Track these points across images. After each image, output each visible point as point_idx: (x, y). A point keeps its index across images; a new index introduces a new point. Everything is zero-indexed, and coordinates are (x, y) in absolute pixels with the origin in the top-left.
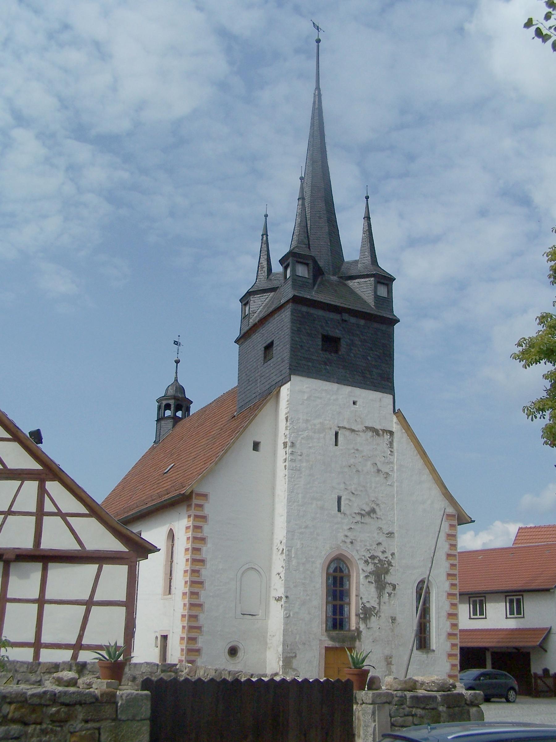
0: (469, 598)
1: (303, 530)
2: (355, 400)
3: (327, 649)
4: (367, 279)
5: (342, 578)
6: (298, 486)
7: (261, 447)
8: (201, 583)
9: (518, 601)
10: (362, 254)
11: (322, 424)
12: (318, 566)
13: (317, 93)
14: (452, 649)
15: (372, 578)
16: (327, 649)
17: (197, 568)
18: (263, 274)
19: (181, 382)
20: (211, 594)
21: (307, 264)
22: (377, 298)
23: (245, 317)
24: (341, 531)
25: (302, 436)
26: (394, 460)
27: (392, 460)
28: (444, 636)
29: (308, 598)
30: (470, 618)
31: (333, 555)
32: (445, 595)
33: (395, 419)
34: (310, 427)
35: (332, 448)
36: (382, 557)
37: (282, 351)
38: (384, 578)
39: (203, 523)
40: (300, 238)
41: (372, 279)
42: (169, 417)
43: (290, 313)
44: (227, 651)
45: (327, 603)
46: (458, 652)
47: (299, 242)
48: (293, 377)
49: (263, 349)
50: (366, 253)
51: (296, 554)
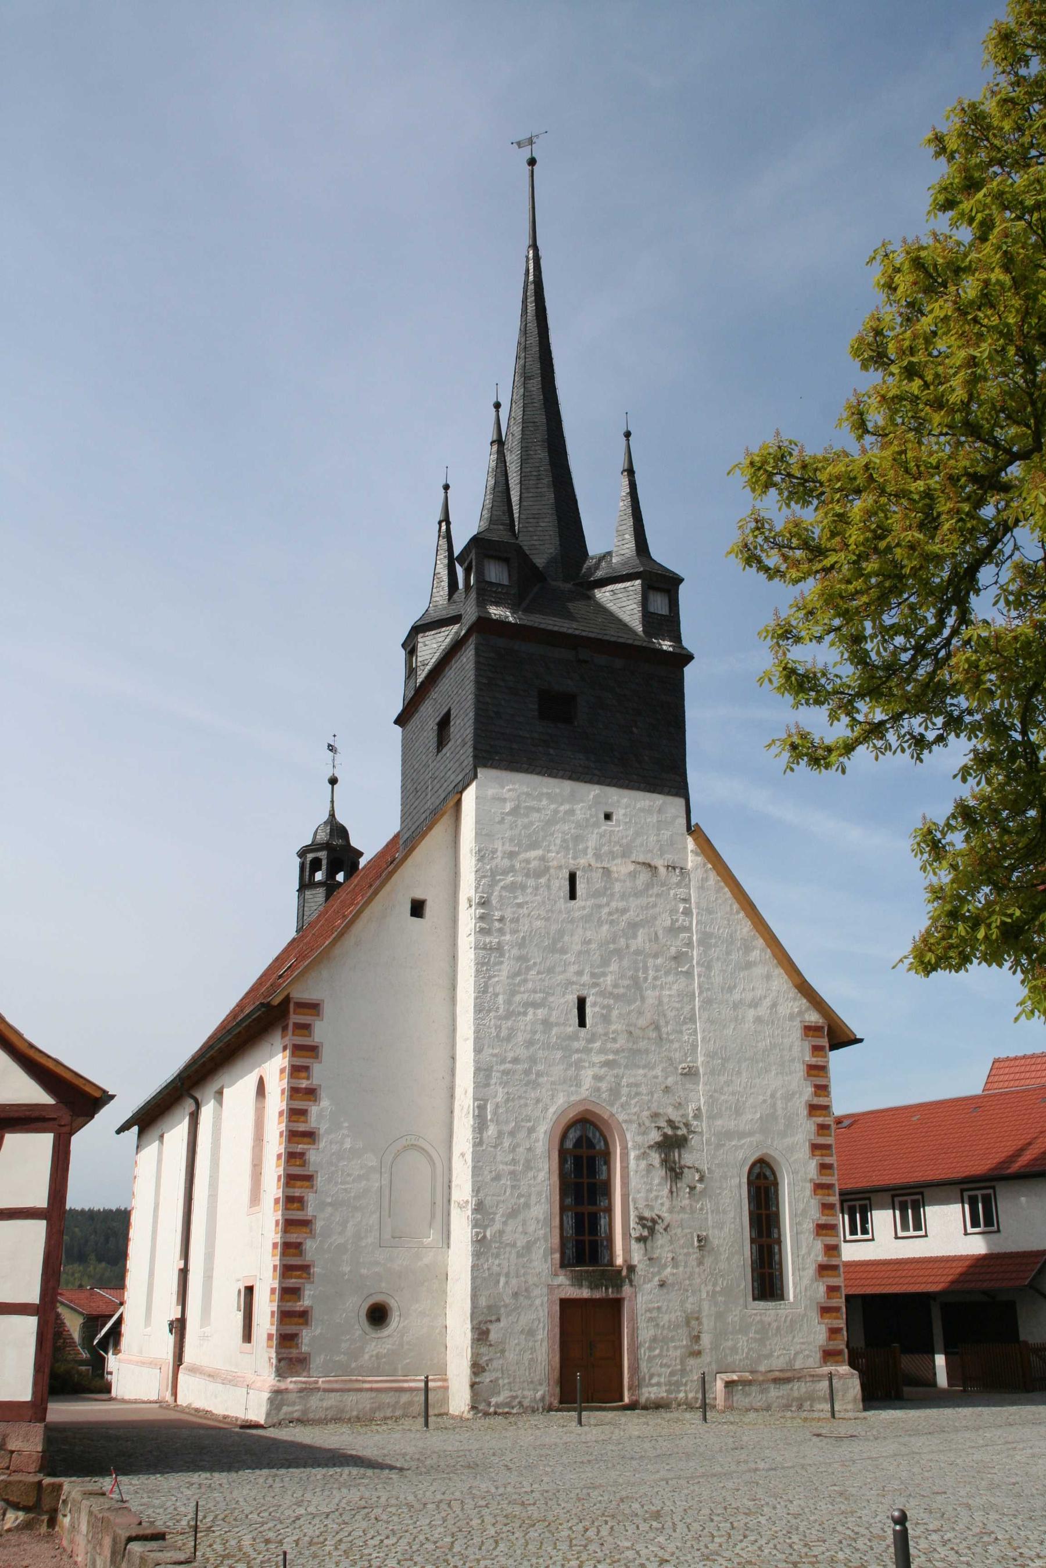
0: (893, 1196)
1: (508, 1066)
2: (609, 810)
3: (566, 1304)
4: (628, 584)
5: (592, 1160)
6: (496, 979)
7: (428, 910)
8: (309, 1178)
9: (987, 1202)
10: (620, 538)
11: (542, 859)
12: (541, 1136)
13: (531, 255)
14: (829, 1298)
15: (656, 1158)
16: (566, 1304)
17: (300, 1148)
18: (441, 593)
19: (340, 818)
20: (329, 1200)
21: (506, 560)
22: (647, 616)
23: (411, 671)
24: (587, 1064)
25: (502, 884)
26: (691, 923)
27: (687, 924)
28: (811, 1270)
29: (522, 1200)
30: (897, 1238)
31: (571, 1114)
32: (809, 1187)
33: (690, 843)
34: (518, 866)
35: (562, 903)
36: (675, 1116)
37: (463, 728)
38: (680, 1155)
39: (311, 1060)
40: (495, 513)
41: (638, 582)
42: (320, 884)
43: (473, 652)
44: (363, 1312)
45: (563, 1209)
46: (840, 1302)
47: (492, 521)
48: (481, 773)
49: (436, 727)
50: (627, 536)
51: (495, 1113)
